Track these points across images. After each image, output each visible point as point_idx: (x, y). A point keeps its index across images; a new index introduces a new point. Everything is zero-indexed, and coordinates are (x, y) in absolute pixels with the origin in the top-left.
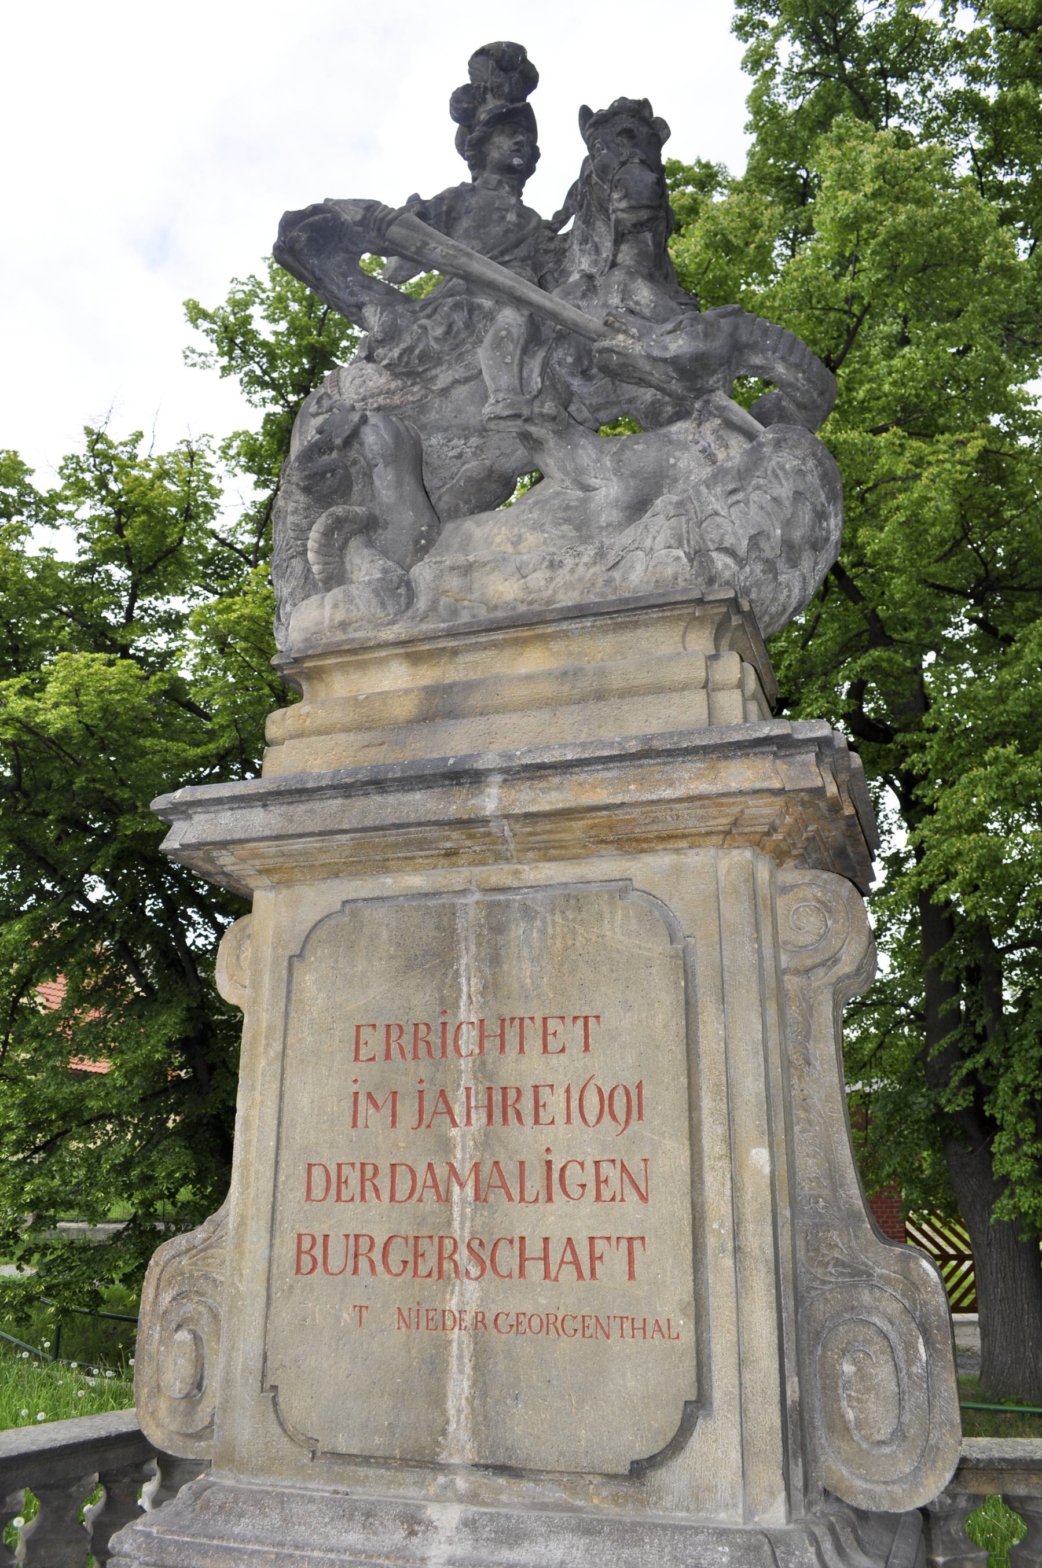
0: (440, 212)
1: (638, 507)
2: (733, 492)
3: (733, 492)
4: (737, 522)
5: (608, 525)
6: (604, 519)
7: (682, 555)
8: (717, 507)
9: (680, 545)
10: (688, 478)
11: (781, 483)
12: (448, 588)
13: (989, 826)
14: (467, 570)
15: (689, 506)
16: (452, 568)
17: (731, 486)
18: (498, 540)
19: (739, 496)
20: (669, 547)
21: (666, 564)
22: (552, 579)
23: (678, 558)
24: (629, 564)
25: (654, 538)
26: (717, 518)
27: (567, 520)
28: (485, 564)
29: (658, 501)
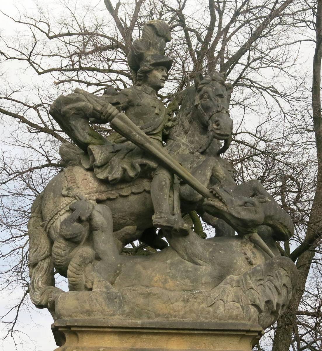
0: (232, 132)
1: (220, 278)
2: (260, 280)
3: (260, 280)
4: (260, 294)
5: (205, 283)
6: (203, 280)
7: (239, 306)
8: (253, 286)
9: (238, 302)
10: (241, 269)
11: (278, 280)
12: (139, 303)
13: (63, 245)
14: (148, 295)
15: (241, 283)
16: (141, 294)
17: (258, 278)
18: (155, 279)
19: (262, 282)
20: (234, 301)
21: (234, 310)
22: (185, 307)
23: (238, 308)
24: (217, 306)
25: (228, 296)
26: (253, 291)
27: (188, 277)
28: (155, 295)
29: (228, 277)
